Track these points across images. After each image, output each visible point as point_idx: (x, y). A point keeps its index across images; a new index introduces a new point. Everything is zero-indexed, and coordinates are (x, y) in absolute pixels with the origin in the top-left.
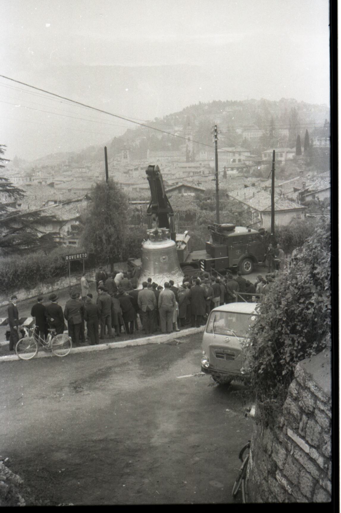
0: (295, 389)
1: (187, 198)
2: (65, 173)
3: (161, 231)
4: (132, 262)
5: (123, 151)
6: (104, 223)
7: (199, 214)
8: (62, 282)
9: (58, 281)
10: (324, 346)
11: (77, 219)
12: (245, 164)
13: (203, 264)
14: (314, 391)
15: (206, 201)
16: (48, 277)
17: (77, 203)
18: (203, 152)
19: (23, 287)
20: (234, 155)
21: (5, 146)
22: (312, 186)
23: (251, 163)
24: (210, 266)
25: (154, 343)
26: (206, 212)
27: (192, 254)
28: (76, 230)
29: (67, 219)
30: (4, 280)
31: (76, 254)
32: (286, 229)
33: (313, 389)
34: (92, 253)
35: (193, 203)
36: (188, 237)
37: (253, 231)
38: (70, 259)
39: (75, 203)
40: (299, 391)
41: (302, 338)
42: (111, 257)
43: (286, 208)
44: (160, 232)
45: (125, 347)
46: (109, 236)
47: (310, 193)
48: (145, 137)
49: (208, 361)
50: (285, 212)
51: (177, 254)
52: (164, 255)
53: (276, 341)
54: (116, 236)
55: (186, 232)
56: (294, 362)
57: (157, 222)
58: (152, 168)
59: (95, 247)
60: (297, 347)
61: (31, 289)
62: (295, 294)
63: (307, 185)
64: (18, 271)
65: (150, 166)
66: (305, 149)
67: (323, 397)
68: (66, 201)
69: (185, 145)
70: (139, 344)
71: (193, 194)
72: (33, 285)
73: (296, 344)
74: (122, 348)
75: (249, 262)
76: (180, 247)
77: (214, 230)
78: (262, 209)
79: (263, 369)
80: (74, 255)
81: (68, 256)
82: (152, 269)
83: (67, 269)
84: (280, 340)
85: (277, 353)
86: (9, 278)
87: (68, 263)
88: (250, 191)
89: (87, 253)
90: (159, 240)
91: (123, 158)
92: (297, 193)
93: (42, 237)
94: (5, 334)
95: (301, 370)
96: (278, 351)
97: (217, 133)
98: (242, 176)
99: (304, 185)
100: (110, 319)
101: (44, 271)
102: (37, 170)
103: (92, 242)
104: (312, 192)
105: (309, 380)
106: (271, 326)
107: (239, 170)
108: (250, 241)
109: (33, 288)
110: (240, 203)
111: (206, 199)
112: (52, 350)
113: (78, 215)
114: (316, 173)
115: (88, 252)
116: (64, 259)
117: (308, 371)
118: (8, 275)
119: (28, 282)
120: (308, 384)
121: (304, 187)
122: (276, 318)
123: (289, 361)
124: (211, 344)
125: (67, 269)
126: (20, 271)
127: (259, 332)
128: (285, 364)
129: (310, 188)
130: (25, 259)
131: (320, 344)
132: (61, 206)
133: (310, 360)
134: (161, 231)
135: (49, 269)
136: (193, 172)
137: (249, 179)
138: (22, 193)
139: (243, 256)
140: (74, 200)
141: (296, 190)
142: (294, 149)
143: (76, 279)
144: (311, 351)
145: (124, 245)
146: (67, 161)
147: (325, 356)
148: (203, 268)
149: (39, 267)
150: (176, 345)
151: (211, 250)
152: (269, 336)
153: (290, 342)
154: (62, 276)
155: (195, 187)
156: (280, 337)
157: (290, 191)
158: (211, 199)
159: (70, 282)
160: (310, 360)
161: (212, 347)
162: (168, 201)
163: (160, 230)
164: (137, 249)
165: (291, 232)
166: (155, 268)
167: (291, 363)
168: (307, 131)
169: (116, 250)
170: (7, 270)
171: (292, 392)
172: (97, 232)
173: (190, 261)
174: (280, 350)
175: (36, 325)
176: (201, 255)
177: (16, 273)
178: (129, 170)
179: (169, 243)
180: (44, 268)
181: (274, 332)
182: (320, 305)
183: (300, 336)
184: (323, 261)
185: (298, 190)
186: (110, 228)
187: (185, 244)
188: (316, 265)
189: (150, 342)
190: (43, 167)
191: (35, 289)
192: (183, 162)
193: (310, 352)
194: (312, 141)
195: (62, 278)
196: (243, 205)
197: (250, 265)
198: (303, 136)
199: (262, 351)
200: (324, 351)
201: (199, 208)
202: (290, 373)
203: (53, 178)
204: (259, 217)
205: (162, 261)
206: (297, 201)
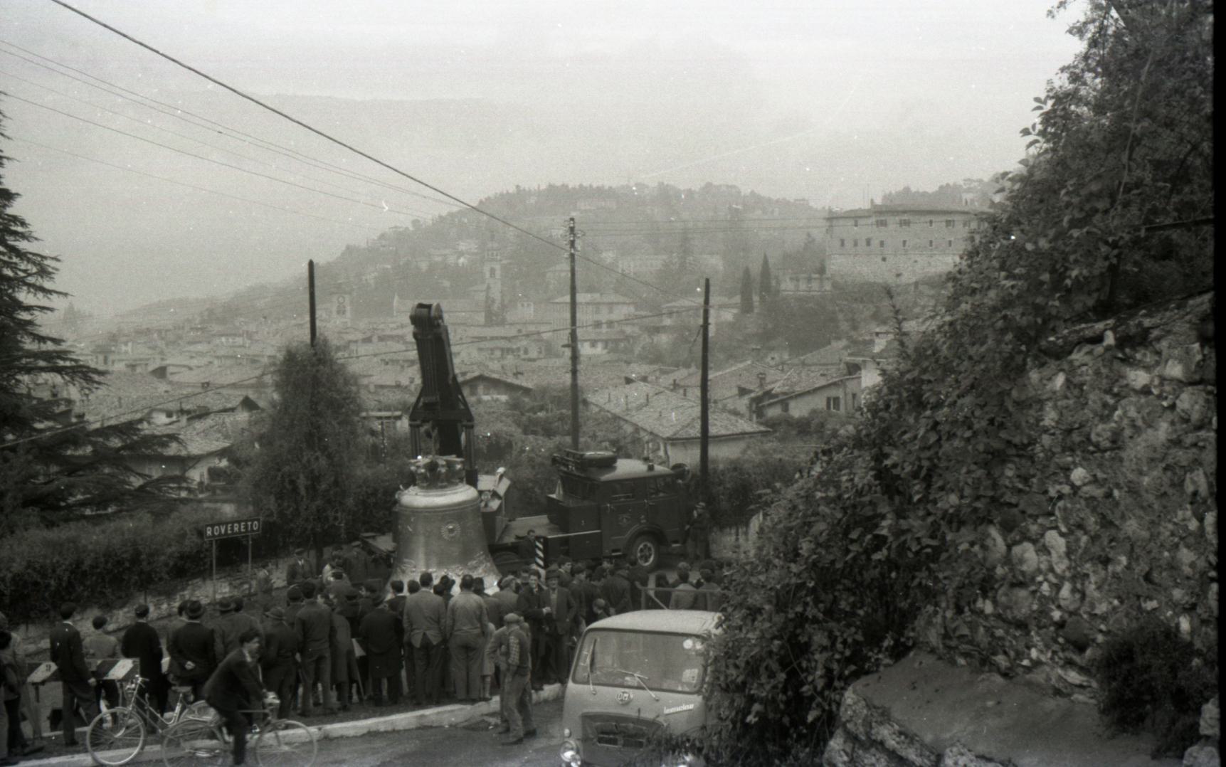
0: (842, 753)
1: (491, 407)
2: (192, 348)
3: (444, 463)
4: (370, 541)
5: (334, 299)
6: (304, 446)
7: (520, 444)
8: (194, 591)
9: (183, 589)
10: (910, 643)
11: (222, 453)
12: (622, 332)
13: (541, 546)
14: (896, 745)
15: (535, 413)
16: (161, 579)
17: (225, 415)
18: (526, 304)
19: (96, 603)
20: (597, 312)
21: (56, 259)
22: (778, 384)
23: (636, 329)
24: (554, 551)
25: (435, 725)
26: (536, 440)
27: (514, 524)
28: (219, 481)
29: (200, 452)
30: (48, 586)
31: (233, 523)
32: (735, 466)
33: (891, 743)
34: (271, 520)
35: (504, 418)
36: (506, 483)
37: (659, 469)
38: (216, 534)
39: (219, 415)
40: (855, 755)
41: (853, 630)
42: (319, 530)
43: (723, 432)
44: (443, 466)
45: (363, 735)
46: (315, 479)
47: (776, 400)
48: (389, 267)
49: (578, 752)
50: (720, 441)
51: (480, 519)
52: (451, 522)
53: (789, 640)
54: (333, 479)
55: (501, 470)
56: (835, 689)
57: (435, 442)
58: (425, 311)
59: (279, 505)
60: (842, 653)
61: (115, 608)
62: (836, 522)
63: (768, 379)
64: (83, 563)
65: (421, 306)
66: (762, 299)
67: (921, 755)
68: (195, 411)
69: (485, 287)
70: (397, 728)
71: (504, 398)
72: (120, 598)
73: (839, 646)
74: (355, 737)
75: (649, 545)
76: (486, 505)
77: (567, 466)
78: (668, 433)
79: (757, 714)
80: (227, 523)
81: (212, 526)
82: (421, 556)
83: (207, 560)
84: (800, 638)
85: (794, 668)
86: (60, 579)
87: (211, 543)
88: (637, 392)
89: (258, 520)
90: (440, 484)
91: (334, 315)
92: (745, 400)
93: (141, 488)
94: (49, 718)
95: (859, 701)
96: (795, 665)
97: (575, 235)
98: (617, 361)
99: (762, 379)
100: (327, 667)
101: (149, 563)
102: (125, 339)
103: (271, 493)
104: (781, 397)
105: (881, 723)
106: (777, 605)
107: (610, 345)
108: (652, 494)
109: (121, 607)
110: (616, 418)
111: (533, 410)
112: (181, 741)
113: (227, 444)
114: (786, 357)
115: (262, 519)
116: (201, 534)
117: (876, 703)
118: (59, 571)
119: (108, 591)
120: (878, 733)
121: (761, 385)
122: (788, 585)
123: (823, 689)
124: (585, 710)
125: (207, 560)
126: (88, 562)
127: (745, 624)
128: (812, 695)
129: (777, 388)
130: (103, 532)
131: (903, 640)
132: (184, 419)
133: (880, 678)
134: (444, 463)
135: (162, 558)
136: (502, 350)
137: (634, 366)
138: (96, 377)
139: (635, 528)
140: (215, 409)
141: (743, 392)
142: (737, 299)
143: (230, 584)
144: (880, 656)
145: (350, 502)
146: (198, 320)
147: (916, 665)
148: (540, 558)
149: (137, 553)
150: (487, 729)
151: (559, 515)
152: (774, 629)
153: (825, 642)
154: (194, 576)
155: (509, 380)
156: (798, 631)
157: (729, 394)
158: (547, 411)
159: (215, 592)
160: (880, 678)
161: (588, 718)
162: (461, 394)
163: (441, 461)
164: (381, 513)
165: (748, 474)
166: (427, 554)
167: (826, 693)
168: (765, 257)
169: (331, 514)
170: (54, 561)
171: (834, 762)
172: (286, 469)
173: (510, 539)
174: (800, 663)
175: (142, 675)
176: (538, 525)
177: (78, 566)
178: (350, 342)
179: (461, 494)
180: (151, 555)
181: (786, 617)
182: (903, 538)
183: (849, 626)
184: (906, 437)
185: (750, 391)
186: (317, 458)
187: (500, 498)
188: (887, 449)
189: (425, 722)
190: (139, 332)
191: (126, 610)
192: (479, 326)
193: (877, 660)
194: (778, 283)
195: (195, 581)
196: (622, 423)
197: (653, 550)
198: (756, 269)
199: (753, 669)
200: (911, 654)
201: (520, 430)
202: (825, 717)
203: (162, 359)
204: (661, 453)
205: (446, 535)
206: (747, 415)
